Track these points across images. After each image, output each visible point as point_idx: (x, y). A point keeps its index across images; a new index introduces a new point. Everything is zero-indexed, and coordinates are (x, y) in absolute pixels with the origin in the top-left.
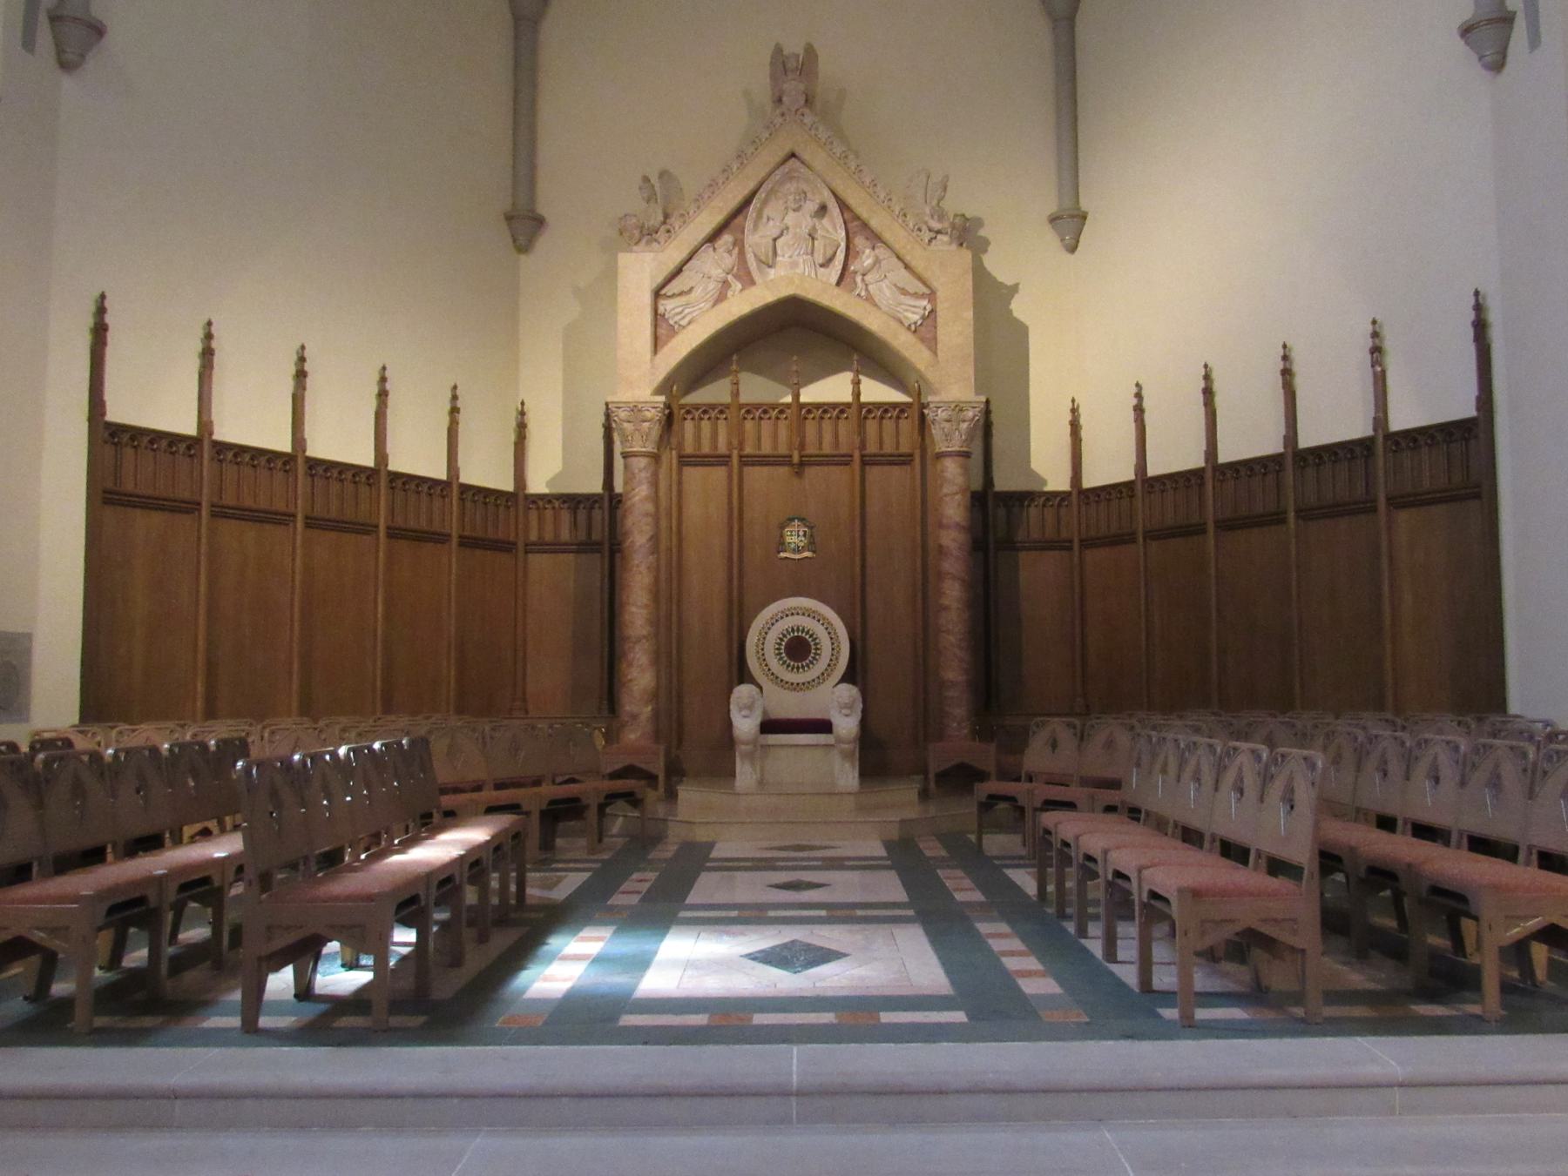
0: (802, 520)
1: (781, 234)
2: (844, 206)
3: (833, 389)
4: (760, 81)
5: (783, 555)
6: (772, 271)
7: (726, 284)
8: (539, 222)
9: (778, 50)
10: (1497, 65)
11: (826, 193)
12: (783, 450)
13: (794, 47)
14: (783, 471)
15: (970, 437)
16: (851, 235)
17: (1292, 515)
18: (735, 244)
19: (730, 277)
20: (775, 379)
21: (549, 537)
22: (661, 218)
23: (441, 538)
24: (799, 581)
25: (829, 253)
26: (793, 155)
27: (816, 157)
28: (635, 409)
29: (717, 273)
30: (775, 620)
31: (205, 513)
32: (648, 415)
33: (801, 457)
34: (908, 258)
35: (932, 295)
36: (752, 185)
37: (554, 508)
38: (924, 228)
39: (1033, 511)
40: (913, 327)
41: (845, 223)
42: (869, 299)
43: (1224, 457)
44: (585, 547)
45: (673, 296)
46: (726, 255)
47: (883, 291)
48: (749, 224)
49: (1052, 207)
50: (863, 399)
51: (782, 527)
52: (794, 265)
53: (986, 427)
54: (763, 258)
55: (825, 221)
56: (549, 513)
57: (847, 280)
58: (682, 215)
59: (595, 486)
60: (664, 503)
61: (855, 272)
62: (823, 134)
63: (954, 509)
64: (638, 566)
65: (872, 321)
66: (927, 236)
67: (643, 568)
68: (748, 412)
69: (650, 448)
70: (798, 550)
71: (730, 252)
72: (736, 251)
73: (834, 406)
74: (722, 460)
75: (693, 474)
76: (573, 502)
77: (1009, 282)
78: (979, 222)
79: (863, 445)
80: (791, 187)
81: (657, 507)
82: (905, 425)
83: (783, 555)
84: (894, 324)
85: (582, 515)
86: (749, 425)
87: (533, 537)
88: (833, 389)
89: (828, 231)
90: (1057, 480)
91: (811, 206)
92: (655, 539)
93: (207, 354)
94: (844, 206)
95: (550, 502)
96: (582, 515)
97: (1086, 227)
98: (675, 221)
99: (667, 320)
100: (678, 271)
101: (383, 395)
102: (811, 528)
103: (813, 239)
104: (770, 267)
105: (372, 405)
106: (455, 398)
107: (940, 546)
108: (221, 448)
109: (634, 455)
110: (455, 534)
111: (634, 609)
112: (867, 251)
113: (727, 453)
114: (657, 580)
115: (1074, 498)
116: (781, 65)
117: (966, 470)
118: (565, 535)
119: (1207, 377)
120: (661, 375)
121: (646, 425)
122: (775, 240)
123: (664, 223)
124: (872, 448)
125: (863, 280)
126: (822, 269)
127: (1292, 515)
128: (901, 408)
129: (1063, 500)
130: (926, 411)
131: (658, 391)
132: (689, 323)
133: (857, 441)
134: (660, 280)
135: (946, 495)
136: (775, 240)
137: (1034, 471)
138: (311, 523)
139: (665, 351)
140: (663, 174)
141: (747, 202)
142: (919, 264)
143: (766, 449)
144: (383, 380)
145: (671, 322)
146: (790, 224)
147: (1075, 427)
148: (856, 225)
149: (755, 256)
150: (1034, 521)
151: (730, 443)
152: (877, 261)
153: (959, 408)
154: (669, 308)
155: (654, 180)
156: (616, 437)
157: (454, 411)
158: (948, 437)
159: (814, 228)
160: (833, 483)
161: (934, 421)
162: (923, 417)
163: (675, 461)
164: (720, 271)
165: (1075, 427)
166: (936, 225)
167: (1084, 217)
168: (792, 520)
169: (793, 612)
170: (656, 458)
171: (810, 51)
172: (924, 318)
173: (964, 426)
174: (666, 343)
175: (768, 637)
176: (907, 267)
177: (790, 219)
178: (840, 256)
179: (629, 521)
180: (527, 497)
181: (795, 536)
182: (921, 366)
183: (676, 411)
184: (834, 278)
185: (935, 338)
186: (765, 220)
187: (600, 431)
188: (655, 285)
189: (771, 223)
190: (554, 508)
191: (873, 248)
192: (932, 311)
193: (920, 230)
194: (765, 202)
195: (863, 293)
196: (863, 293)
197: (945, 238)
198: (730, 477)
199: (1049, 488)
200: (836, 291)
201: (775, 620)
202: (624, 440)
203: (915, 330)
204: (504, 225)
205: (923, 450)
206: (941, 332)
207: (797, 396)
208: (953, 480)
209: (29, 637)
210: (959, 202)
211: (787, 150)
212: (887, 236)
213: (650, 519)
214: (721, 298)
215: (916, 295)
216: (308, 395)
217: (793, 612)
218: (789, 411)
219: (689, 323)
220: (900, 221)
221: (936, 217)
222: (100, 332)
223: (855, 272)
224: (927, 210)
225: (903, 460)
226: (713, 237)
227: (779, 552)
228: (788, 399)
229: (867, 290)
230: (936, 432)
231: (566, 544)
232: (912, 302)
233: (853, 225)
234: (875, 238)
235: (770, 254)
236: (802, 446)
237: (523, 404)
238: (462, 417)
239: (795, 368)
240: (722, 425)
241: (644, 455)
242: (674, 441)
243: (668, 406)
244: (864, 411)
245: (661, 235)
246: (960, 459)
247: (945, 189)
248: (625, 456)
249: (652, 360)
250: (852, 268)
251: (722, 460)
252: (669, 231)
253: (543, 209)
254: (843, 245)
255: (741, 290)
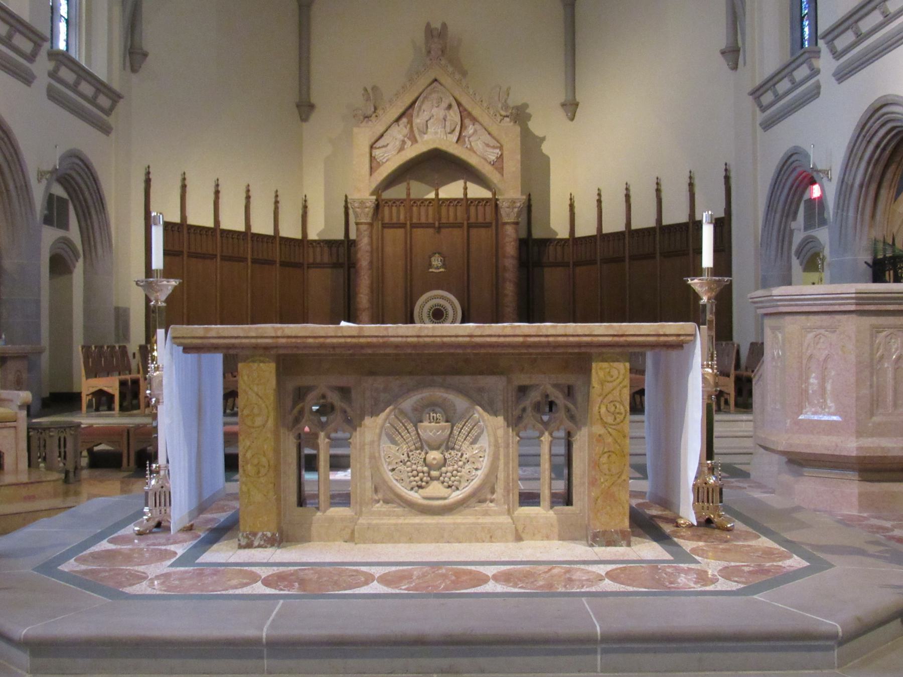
0: (439, 253)
1: (430, 119)
2: (459, 104)
3: (452, 190)
4: (420, 36)
5: (431, 270)
6: (426, 136)
7: (404, 142)
8: (312, 107)
9: (428, 25)
10: (735, 67)
11: (451, 98)
12: (430, 221)
13: (437, 25)
14: (431, 231)
15: (519, 214)
16: (463, 118)
17: (658, 255)
18: (408, 123)
19: (406, 139)
20: (426, 183)
21: (318, 260)
22: (373, 110)
23: (271, 263)
24: (438, 282)
25: (453, 127)
26: (436, 80)
27: (446, 80)
28: (362, 203)
29: (400, 137)
30: (427, 301)
31: (185, 256)
32: (368, 205)
33: (439, 224)
34: (490, 129)
35: (501, 148)
36: (416, 95)
37: (321, 247)
38: (498, 115)
39: (551, 248)
40: (492, 163)
41: (460, 112)
42: (471, 149)
43: (634, 227)
44: (335, 265)
45: (379, 148)
46: (404, 128)
47: (478, 145)
48: (415, 113)
49: (562, 98)
50: (470, 196)
51: (430, 257)
52: (436, 133)
53: (529, 206)
54: (421, 129)
55: (451, 112)
56: (318, 249)
57: (461, 140)
58: (383, 109)
59: (340, 236)
60: (375, 247)
61: (465, 136)
62: (450, 69)
63: (510, 248)
64: (364, 275)
65: (473, 160)
66: (499, 118)
67: (366, 277)
68: (415, 202)
69: (369, 220)
70: (437, 268)
71: (406, 127)
72: (409, 126)
73: (455, 200)
74: (402, 226)
75: (389, 233)
76: (330, 243)
77: (541, 136)
78: (526, 106)
79: (468, 218)
80: (435, 96)
81: (372, 248)
82: (488, 209)
83: (431, 270)
84: (483, 161)
85: (334, 250)
86: (415, 209)
87: (311, 261)
88: (452, 190)
89: (452, 117)
90: (563, 233)
91: (444, 105)
92: (371, 263)
93: (184, 187)
94: (459, 104)
95: (319, 243)
96: (334, 250)
97: (578, 109)
98: (380, 112)
99: (376, 160)
100: (382, 136)
101: (248, 198)
102: (444, 258)
103: (445, 120)
104: (425, 134)
105: (243, 202)
106: (277, 196)
107: (505, 266)
108: (191, 227)
109: (361, 223)
110: (278, 261)
111: (362, 296)
112: (471, 126)
113: (404, 222)
114: (372, 283)
115: (571, 243)
116: (430, 32)
117: (517, 231)
118: (326, 259)
119: (627, 189)
120: (374, 185)
121: (367, 209)
122: (427, 121)
123: (375, 112)
124: (472, 220)
125: (469, 140)
126: (450, 135)
127: (658, 255)
128: (487, 200)
129: (566, 242)
130: (498, 202)
131: (372, 194)
132: (387, 161)
133: (466, 216)
134: (373, 140)
135: (507, 242)
136: (427, 121)
137: (552, 229)
138: (223, 258)
139: (376, 174)
140: (375, 88)
141: (414, 103)
142: (495, 132)
143: (423, 220)
144: (248, 191)
145: (378, 160)
146: (434, 114)
147: (572, 206)
148: (465, 115)
149: (418, 128)
150: (551, 253)
151: (406, 218)
152: (475, 131)
153: (513, 202)
154: (377, 153)
155: (369, 90)
156: (351, 212)
157: (276, 202)
158: (508, 215)
159: (446, 116)
160: (457, 235)
161: (502, 208)
162: (496, 205)
163: (380, 226)
164: (401, 136)
165: (572, 206)
166: (504, 113)
167: (577, 105)
168: (436, 253)
169: (435, 297)
170: (371, 225)
171: (444, 26)
172: (497, 158)
173: (516, 210)
174: (376, 170)
175: (424, 309)
176: (489, 134)
177: (435, 111)
178: (458, 128)
179: (359, 255)
180: (308, 241)
181: (436, 261)
182: (495, 181)
183: (380, 203)
184: (455, 139)
185: (502, 168)
186: (422, 111)
187: (343, 210)
188: (370, 143)
189: (425, 113)
190: (321, 247)
191: (474, 125)
192: (502, 155)
193: (495, 115)
194: (423, 102)
195: (469, 146)
196: (469, 146)
197: (507, 119)
198: (406, 233)
199: (559, 236)
200: (456, 146)
201: (427, 301)
202: (356, 216)
203: (493, 164)
204: (296, 110)
205: (497, 220)
206: (505, 165)
207: (437, 194)
208: (510, 236)
209: (129, 309)
210: (515, 100)
211: (433, 77)
212: (480, 119)
213: (368, 254)
214: (401, 149)
215: (494, 147)
216: (220, 201)
217: (435, 297)
218: (433, 202)
219: (387, 161)
220: (486, 111)
221: (504, 108)
222: (148, 182)
223: (465, 136)
224: (500, 106)
225: (487, 225)
226: (398, 120)
227: (429, 269)
228: (432, 195)
229: (470, 144)
230: (503, 212)
231: (326, 264)
232: (491, 150)
233: (465, 114)
234: (474, 120)
235: (425, 127)
236: (440, 219)
237: (306, 196)
238: (280, 205)
239: (436, 182)
240: (402, 210)
241: (365, 223)
242: (380, 218)
243: (377, 200)
244: (469, 202)
245: (373, 118)
246: (514, 226)
247: (508, 95)
248: (357, 224)
249: (369, 179)
250: (464, 134)
251: (402, 226)
252: (376, 116)
253: (313, 100)
254: (459, 123)
255: (412, 145)
